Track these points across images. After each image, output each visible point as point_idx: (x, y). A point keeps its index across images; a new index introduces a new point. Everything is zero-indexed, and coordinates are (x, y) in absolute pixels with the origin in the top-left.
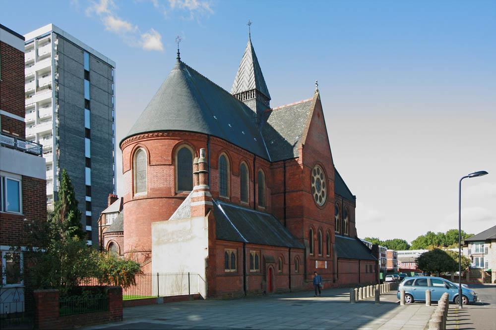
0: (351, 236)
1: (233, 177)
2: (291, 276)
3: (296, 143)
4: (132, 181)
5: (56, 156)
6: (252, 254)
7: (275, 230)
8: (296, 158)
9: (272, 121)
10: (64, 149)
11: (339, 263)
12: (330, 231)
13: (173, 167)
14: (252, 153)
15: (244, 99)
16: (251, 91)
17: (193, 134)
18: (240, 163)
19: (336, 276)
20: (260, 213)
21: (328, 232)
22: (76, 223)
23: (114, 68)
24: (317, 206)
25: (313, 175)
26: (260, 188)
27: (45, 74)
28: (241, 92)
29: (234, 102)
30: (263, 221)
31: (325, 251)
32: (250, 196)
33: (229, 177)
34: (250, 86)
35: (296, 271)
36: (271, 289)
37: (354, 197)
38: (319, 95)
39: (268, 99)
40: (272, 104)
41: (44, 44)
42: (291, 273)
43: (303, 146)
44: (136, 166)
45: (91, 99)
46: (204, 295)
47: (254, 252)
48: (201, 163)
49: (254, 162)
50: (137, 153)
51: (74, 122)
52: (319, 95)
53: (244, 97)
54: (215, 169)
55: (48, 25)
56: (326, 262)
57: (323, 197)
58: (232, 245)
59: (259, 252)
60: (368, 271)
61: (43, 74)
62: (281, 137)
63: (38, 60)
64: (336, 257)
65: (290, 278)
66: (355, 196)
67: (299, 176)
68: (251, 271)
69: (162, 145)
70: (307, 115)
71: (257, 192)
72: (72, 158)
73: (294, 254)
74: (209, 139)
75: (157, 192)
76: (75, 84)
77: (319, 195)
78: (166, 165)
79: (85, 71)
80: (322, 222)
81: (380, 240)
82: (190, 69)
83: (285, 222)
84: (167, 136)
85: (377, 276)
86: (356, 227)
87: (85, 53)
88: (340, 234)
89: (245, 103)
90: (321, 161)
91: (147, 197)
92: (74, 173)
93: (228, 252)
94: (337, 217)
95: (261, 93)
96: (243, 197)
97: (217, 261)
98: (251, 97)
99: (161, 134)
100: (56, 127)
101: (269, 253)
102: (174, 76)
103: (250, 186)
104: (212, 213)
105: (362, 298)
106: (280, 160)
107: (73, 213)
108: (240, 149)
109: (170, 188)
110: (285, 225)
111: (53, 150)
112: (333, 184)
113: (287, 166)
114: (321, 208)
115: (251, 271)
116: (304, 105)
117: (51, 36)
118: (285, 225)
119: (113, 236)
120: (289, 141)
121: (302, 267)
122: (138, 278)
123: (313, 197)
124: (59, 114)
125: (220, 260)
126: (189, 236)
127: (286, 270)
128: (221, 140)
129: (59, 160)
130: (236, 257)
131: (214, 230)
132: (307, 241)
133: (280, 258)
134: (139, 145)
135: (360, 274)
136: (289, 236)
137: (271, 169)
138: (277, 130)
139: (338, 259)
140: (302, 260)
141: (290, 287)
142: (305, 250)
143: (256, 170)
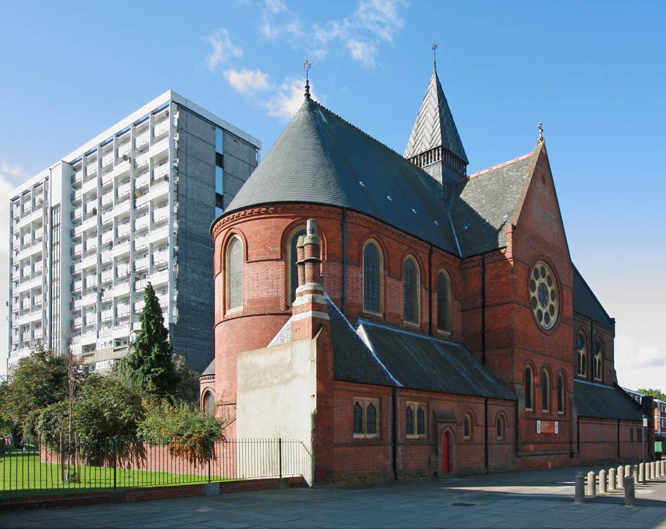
0: (605, 382)
1: (389, 280)
2: (489, 446)
3: (503, 225)
4: (222, 291)
5: (172, 274)
6: (412, 408)
7: (464, 368)
8: (502, 248)
9: (468, 195)
10: (184, 263)
11: (580, 424)
12: (564, 372)
13: (283, 263)
14: (426, 242)
15: (424, 164)
16: (435, 149)
17: (315, 207)
18: (403, 257)
19: (575, 446)
20: (441, 341)
21: (560, 373)
22: (162, 363)
23: (258, 149)
24: (541, 329)
25: (532, 277)
26: (442, 300)
27: (162, 161)
28: (419, 153)
29: (409, 170)
30: (443, 353)
31: (555, 404)
32: (422, 313)
33: (382, 280)
34: (433, 142)
35: (500, 438)
36: (448, 468)
37: (612, 321)
38: (544, 146)
39: (464, 162)
40: (471, 172)
41: (161, 119)
42: (489, 440)
43: (514, 228)
44: (229, 264)
45: (224, 193)
46: (309, 478)
47: (415, 405)
48: (307, 244)
49: (430, 257)
50: (231, 243)
51: (201, 226)
52: (544, 146)
53: (424, 161)
54: (356, 265)
55: (165, 94)
56: (556, 423)
57: (552, 315)
58: (368, 390)
59: (425, 404)
60: (635, 438)
61: (161, 161)
62: (480, 217)
63: (153, 143)
64: (575, 415)
65: (486, 449)
66: (614, 319)
67: (507, 278)
68: (409, 437)
69: (266, 229)
70: (522, 180)
71: (436, 307)
72: (196, 276)
73: (494, 409)
74: (344, 216)
75: (257, 306)
76: (202, 173)
77: (544, 312)
78: (272, 260)
79: (217, 154)
80: (551, 357)
81: (661, 393)
82: (328, 114)
83: (484, 357)
84: (275, 212)
85: (651, 447)
86: (616, 368)
87: (217, 129)
88: (587, 379)
89: (425, 169)
90: (548, 255)
91: (241, 315)
92: (198, 296)
93: (360, 403)
94: (582, 352)
95: (451, 153)
96: (410, 313)
97: (336, 419)
98: (435, 160)
99: (264, 209)
100: (174, 233)
101: (445, 405)
102: (298, 121)
103: (421, 295)
104: (326, 333)
105: (606, 491)
106: (477, 253)
107: (158, 347)
108: (403, 234)
109: (277, 299)
110: (484, 361)
111: (169, 266)
112: (570, 294)
113: (488, 263)
114: (546, 332)
115: (409, 437)
116: (519, 166)
117: (169, 108)
118: (484, 361)
119: (210, 381)
120: (492, 224)
121: (510, 431)
122: (219, 448)
123: (532, 313)
124: (179, 216)
125: (342, 416)
126: (288, 375)
127: (478, 435)
128: (366, 217)
129: (177, 280)
130: (378, 411)
131: (330, 364)
132: (520, 388)
133: (468, 416)
134: (232, 231)
135: (621, 444)
136: (489, 378)
137: (462, 270)
138: (474, 209)
139: (579, 417)
140: (511, 419)
141: (486, 465)
142: (516, 402)
143: (433, 271)
